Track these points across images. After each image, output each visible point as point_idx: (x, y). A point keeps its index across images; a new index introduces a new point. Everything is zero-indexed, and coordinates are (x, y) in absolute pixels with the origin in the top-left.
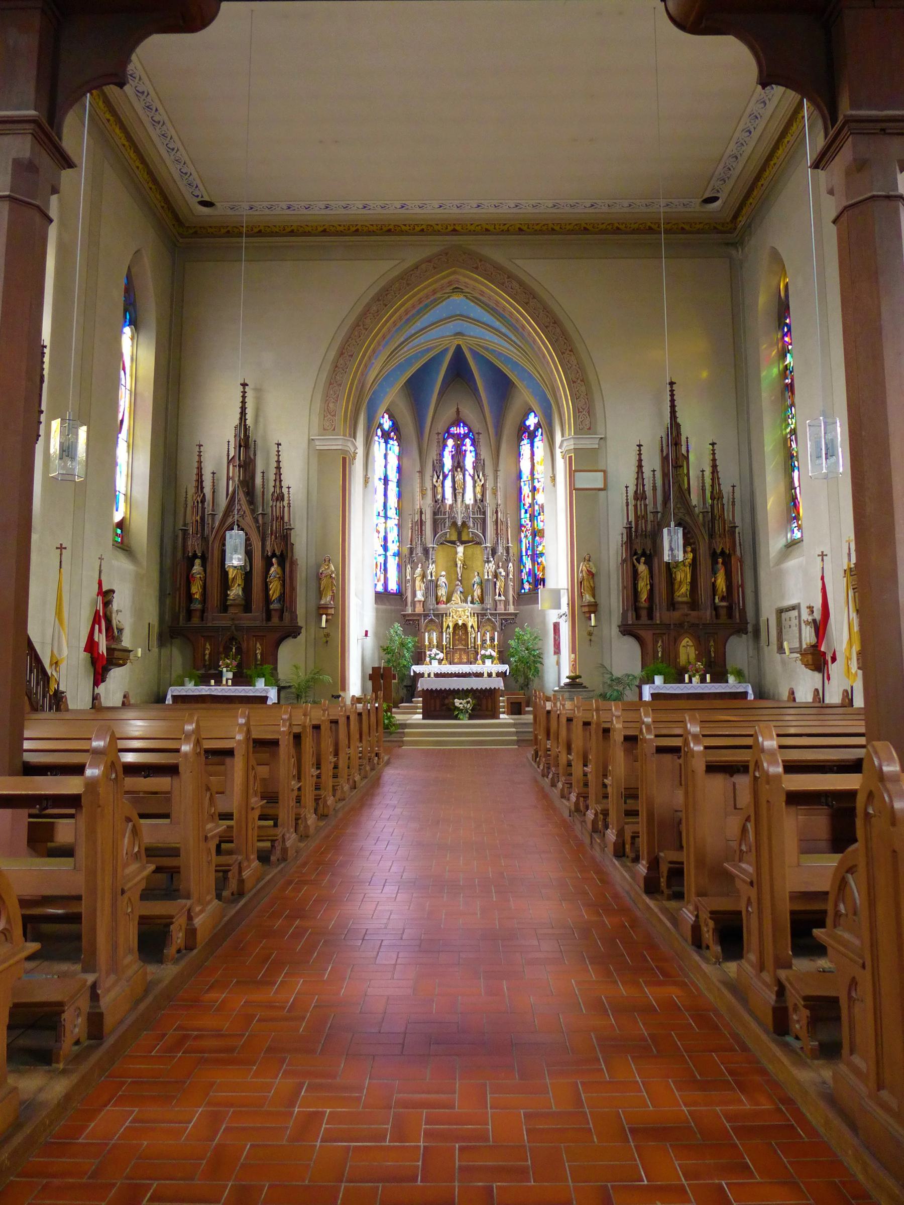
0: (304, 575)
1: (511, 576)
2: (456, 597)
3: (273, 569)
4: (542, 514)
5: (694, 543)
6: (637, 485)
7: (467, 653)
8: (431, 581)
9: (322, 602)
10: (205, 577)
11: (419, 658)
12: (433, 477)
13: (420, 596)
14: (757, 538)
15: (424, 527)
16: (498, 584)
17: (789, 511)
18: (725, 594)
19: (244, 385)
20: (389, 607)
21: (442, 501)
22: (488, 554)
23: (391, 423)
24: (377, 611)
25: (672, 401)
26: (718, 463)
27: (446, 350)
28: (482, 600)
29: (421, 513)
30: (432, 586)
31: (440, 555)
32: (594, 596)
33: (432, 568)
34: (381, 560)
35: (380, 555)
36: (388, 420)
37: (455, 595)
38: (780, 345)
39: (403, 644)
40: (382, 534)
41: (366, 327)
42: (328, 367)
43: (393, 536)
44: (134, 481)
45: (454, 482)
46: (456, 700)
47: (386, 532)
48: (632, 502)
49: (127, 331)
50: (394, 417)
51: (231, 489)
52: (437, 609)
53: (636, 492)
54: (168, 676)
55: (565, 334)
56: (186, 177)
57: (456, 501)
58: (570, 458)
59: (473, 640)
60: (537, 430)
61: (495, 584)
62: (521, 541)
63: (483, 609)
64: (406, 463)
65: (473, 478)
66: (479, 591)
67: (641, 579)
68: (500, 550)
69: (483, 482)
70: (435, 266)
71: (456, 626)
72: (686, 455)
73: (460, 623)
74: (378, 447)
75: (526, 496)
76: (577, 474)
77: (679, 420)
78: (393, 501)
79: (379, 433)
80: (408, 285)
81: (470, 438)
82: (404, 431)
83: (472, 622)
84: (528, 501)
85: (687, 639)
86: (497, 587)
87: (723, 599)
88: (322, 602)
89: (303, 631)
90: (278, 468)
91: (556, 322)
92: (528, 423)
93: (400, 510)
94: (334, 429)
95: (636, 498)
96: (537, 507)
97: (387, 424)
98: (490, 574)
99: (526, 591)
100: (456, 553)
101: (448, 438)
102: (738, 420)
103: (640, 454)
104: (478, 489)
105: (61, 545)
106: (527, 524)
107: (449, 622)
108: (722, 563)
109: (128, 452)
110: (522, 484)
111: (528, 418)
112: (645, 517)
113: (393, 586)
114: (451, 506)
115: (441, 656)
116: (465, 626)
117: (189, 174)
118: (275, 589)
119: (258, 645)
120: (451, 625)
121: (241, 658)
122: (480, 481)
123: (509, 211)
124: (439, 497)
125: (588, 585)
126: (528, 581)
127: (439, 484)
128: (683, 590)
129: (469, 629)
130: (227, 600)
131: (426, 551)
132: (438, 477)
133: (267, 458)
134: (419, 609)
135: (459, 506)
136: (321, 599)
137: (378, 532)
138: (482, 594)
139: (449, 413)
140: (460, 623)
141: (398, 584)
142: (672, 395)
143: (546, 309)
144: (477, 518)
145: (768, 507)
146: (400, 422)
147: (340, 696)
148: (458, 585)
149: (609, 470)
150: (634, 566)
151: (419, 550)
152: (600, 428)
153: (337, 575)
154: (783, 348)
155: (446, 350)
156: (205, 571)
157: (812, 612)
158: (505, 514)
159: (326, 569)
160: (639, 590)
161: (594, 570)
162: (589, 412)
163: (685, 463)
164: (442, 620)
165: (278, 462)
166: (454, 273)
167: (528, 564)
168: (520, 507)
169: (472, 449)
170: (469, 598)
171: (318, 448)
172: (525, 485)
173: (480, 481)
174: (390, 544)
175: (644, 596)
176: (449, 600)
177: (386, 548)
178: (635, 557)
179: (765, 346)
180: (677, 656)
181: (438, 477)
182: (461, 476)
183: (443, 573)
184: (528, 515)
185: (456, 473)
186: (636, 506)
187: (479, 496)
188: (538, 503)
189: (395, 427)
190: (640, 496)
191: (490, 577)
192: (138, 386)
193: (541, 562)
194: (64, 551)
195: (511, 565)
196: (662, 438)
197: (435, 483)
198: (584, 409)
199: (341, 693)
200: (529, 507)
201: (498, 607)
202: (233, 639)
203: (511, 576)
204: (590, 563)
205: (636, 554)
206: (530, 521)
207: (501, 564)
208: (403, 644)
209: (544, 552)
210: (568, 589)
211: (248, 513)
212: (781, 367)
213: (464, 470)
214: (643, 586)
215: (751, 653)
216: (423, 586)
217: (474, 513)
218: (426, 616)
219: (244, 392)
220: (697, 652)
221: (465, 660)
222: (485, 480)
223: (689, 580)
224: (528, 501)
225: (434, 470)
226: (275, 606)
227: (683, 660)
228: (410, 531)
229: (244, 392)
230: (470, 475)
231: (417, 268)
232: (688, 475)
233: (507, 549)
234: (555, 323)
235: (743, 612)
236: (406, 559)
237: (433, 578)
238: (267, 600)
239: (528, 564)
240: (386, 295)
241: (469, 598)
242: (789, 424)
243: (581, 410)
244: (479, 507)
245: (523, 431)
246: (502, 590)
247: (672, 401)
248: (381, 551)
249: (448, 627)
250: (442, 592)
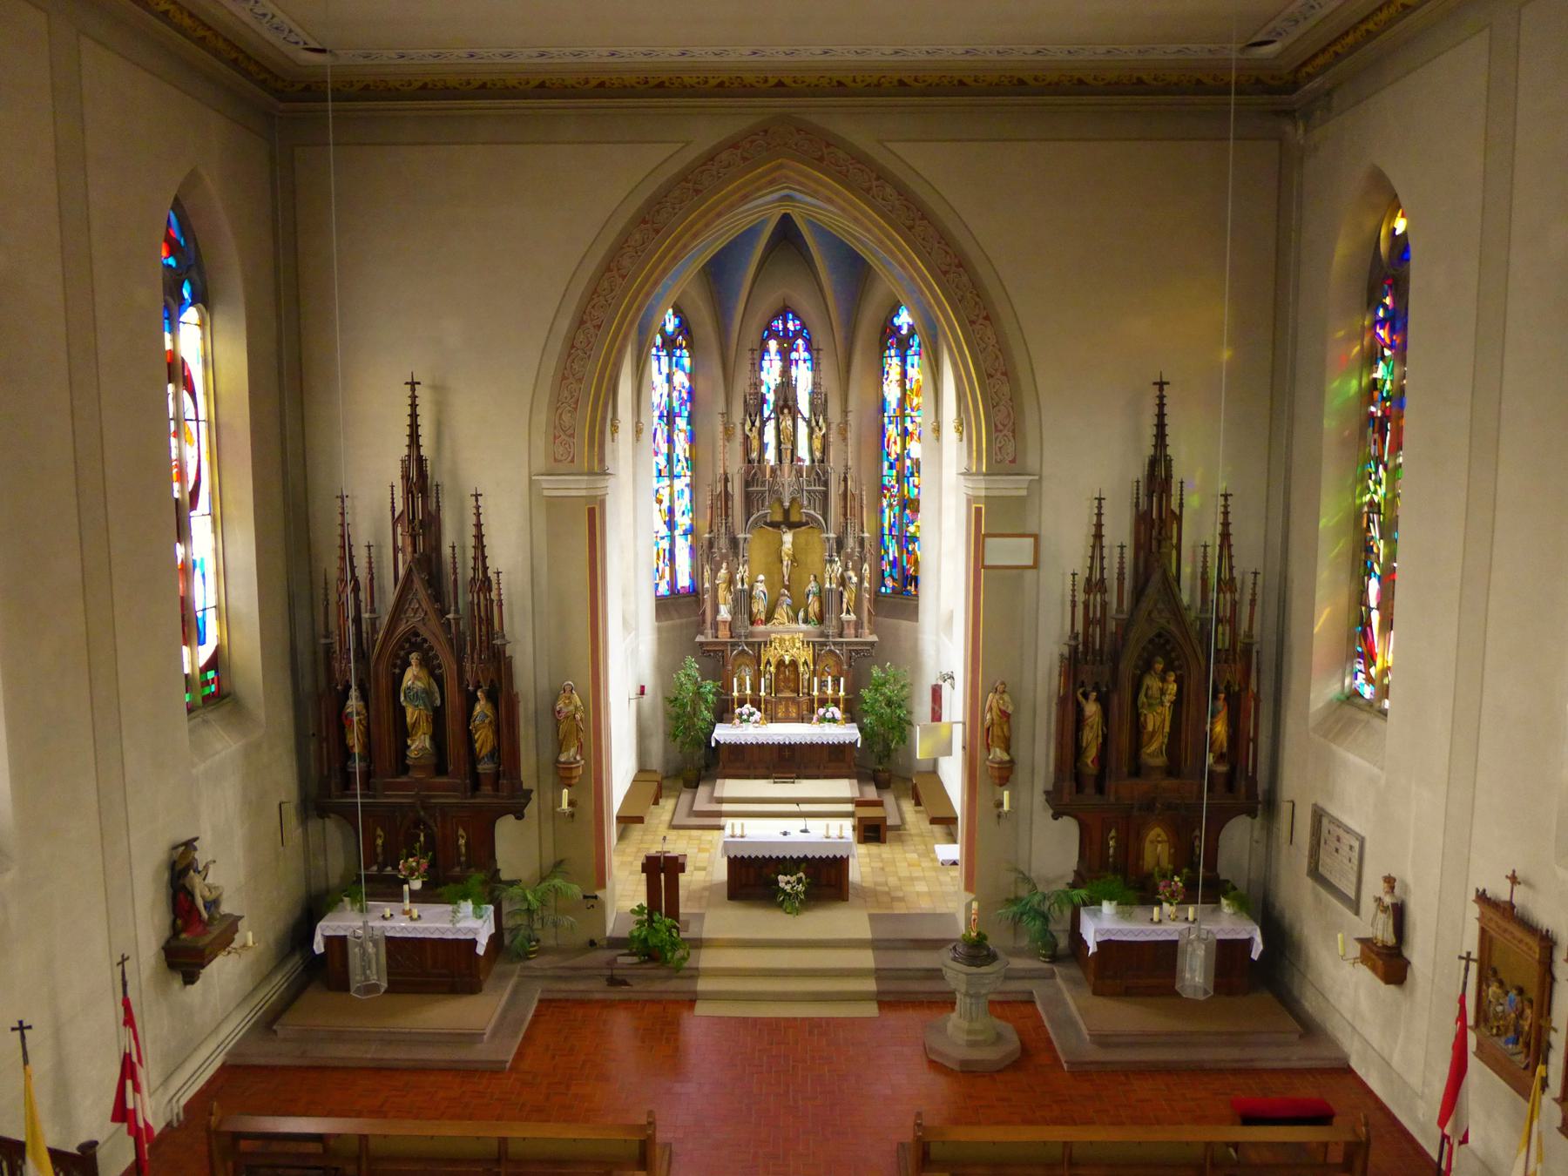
0: (531, 706)
1: (866, 585)
2: (782, 613)
3: (478, 708)
4: (916, 474)
5: (1180, 667)
6: (1091, 568)
7: (798, 704)
8: (743, 591)
9: (563, 758)
10: (368, 716)
11: (724, 712)
12: (743, 425)
13: (724, 614)
14: (1285, 658)
15: (730, 503)
16: (846, 595)
17: (1351, 640)
18: (1225, 750)
19: (413, 384)
20: (678, 621)
21: (759, 461)
22: (831, 549)
23: (677, 321)
24: (659, 630)
25: (1161, 416)
26: (1232, 529)
27: (764, 222)
28: (821, 619)
29: (726, 480)
30: (743, 600)
31: (755, 544)
32: (1007, 749)
33: (743, 571)
34: (665, 544)
35: (662, 538)
36: (672, 318)
37: (779, 610)
38: (1367, 341)
39: (698, 694)
40: (666, 504)
41: (623, 272)
42: (557, 346)
43: (682, 504)
44: (231, 581)
45: (778, 428)
46: (780, 877)
47: (672, 501)
48: (1081, 597)
49: (191, 315)
50: (682, 313)
51: (401, 572)
52: (752, 634)
53: (1089, 580)
54: (322, 863)
55: (976, 286)
56: (266, 20)
57: (780, 461)
58: (978, 510)
59: (806, 684)
60: (912, 336)
61: (841, 594)
62: (882, 512)
63: (822, 635)
64: (701, 386)
65: (809, 423)
66: (816, 606)
67: (1088, 728)
68: (851, 543)
69: (824, 431)
70: (745, 155)
71: (781, 663)
72: (1178, 512)
73: (787, 659)
74: (658, 369)
75: (892, 440)
76: (989, 541)
77: (1169, 451)
78: (682, 446)
79: (659, 341)
80: (697, 192)
81: (804, 339)
82: (698, 332)
83: (805, 655)
84: (896, 449)
85: (1158, 830)
86: (845, 600)
87: (1220, 758)
88: (563, 758)
89: (534, 796)
90: (479, 537)
91: (962, 264)
92: (897, 321)
93: (693, 462)
94: (572, 461)
95: (1088, 590)
96: (908, 463)
97: (671, 325)
98: (834, 580)
99: (889, 591)
100: (781, 543)
101: (769, 337)
102: (1270, 445)
103: (1099, 515)
104: (817, 444)
105: (21, 1022)
106: (893, 487)
107: (771, 654)
108: (1225, 699)
109: (215, 531)
110: (886, 420)
111: (898, 314)
112: (1102, 622)
113: (684, 581)
114: (773, 470)
115: (758, 715)
116: (794, 663)
117: (269, 16)
118: (483, 738)
119: (461, 832)
120: (773, 661)
121: (434, 855)
122: (820, 429)
123: (884, 58)
124: (755, 455)
125: (1000, 733)
126: (891, 576)
127: (754, 434)
128: (1154, 747)
129: (801, 669)
130: (405, 756)
131: (734, 543)
132: (753, 424)
133: (461, 511)
134: (724, 635)
135: (786, 476)
136: (560, 752)
137: (660, 502)
138: (821, 610)
139: (769, 301)
140: (787, 659)
141: (691, 577)
142: (1161, 405)
143: (944, 237)
144: (814, 491)
145: (1316, 630)
146: (689, 312)
147: (596, 897)
148: (784, 595)
149: (1046, 533)
150: (1078, 704)
151: (723, 542)
152: (1032, 461)
153: (586, 712)
154: (1373, 345)
155: (764, 222)
156: (367, 707)
157: (1392, 888)
158: (859, 483)
159: (567, 705)
160: (1084, 744)
161: (1010, 710)
162: (1013, 431)
163: (1175, 526)
164: (759, 651)
165: (478, 526)
166: (781, 166)
167: (893, 550)
168: (882, 457)
169: (806, 355)
170: (801, 614)
171: (546, 493)
172: (890, 422)
173: (820, 429)
174: (678, 517)
175: (1092, 753)
176: (770, 617)
177: (671, 525)
178: (1081, 690)
179: (1341, 334)
180: (1140, 855)
181: (753, 424)
182: (790, 423)
183: (761, 577)
184: (894, 472)
185: (781, 417)
186: (1086, 605)
187: (818, 454)
188: (912, 456)
189: (684, 328)
190: (1095, 585)
191: (834, 586)
192: (221, 411)
193: (914, 549)
194: (26, 1032)
195: (866, 566)
196: (1138, 482)
197: (747, 432)
198: (1004, 426)
199: (599, 893)
200: (897, 460)
201: (846, 632)
202: (417, 823)
203: (866, 585)
204: (1006, 697)
205: (1083, 685)
206: (898, 482)
207: (850, 564)
208: (698, 694)
209: (918, 535)
210: (964, 724)
211: (432, 616)
212: (1365, 381)
213: (794, 412)
214: (1091, 737)
215: (1256, 834)
216: (729, 598)
217: (809, 483)
218: (734, 645)
219: (414, 397)
220: (1172, 851)
221: (794, 715)
222: (828, 428)
223: (1167, 729)
224: (896, 449)
225: (746, 411)
226: (485, 767)
227: (1149, 861)
228: (709, 511)
229: (414, 397)
230: (804, 419)
231: (712, 159)
232: (1179, 548)
233: (861, 542)
234: (960, 265)
235: (1252, 781)
236: (704, 553)
237: (746, 586)
238: (472, 758)
239: (893, 550)
240: (658, 212)
241: (801, 614)
242: (1368, 488)
243: (1000, 427)
244: (817, 474)
245: (889, 335)
246: (852, 604)
247: (1161, 416)
248: (664, 531)
249: (768, 662)
250: (759, 607)
